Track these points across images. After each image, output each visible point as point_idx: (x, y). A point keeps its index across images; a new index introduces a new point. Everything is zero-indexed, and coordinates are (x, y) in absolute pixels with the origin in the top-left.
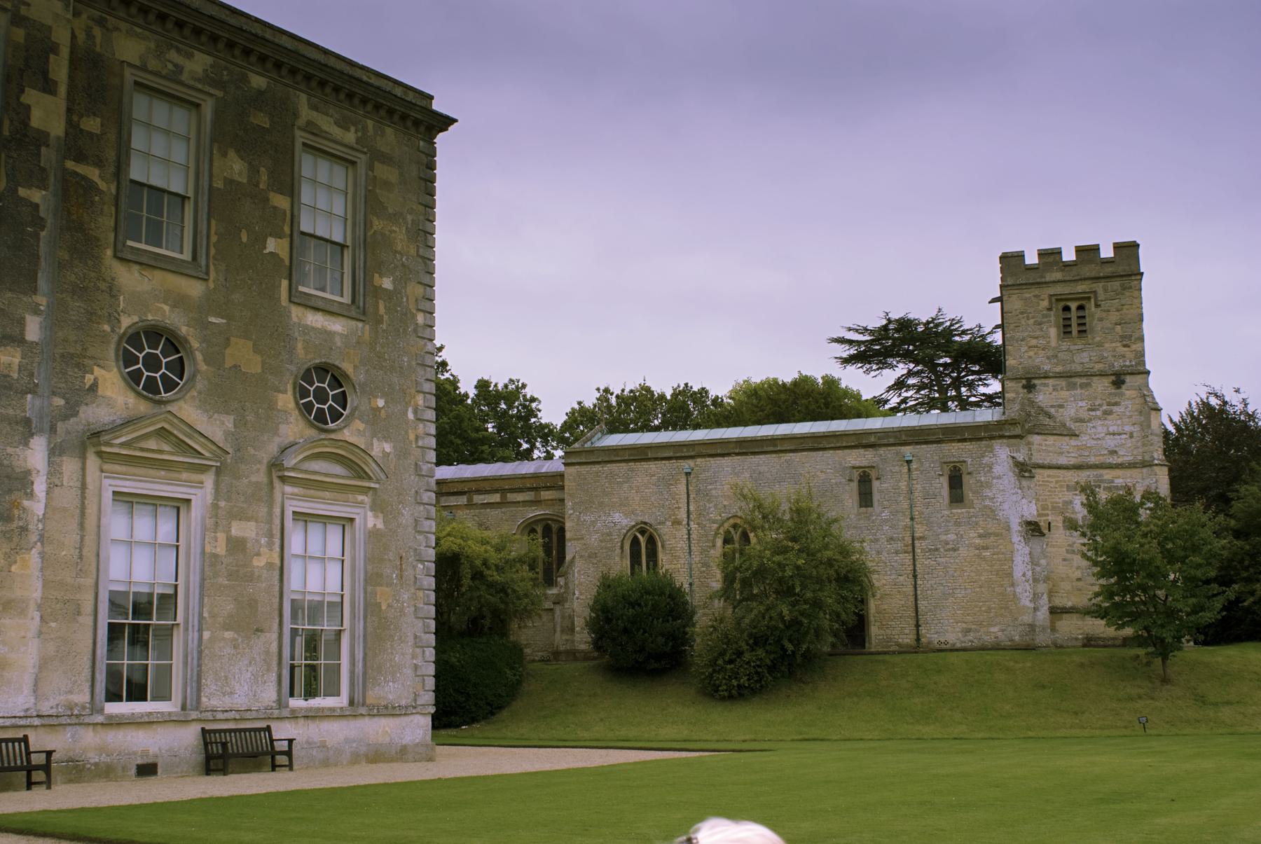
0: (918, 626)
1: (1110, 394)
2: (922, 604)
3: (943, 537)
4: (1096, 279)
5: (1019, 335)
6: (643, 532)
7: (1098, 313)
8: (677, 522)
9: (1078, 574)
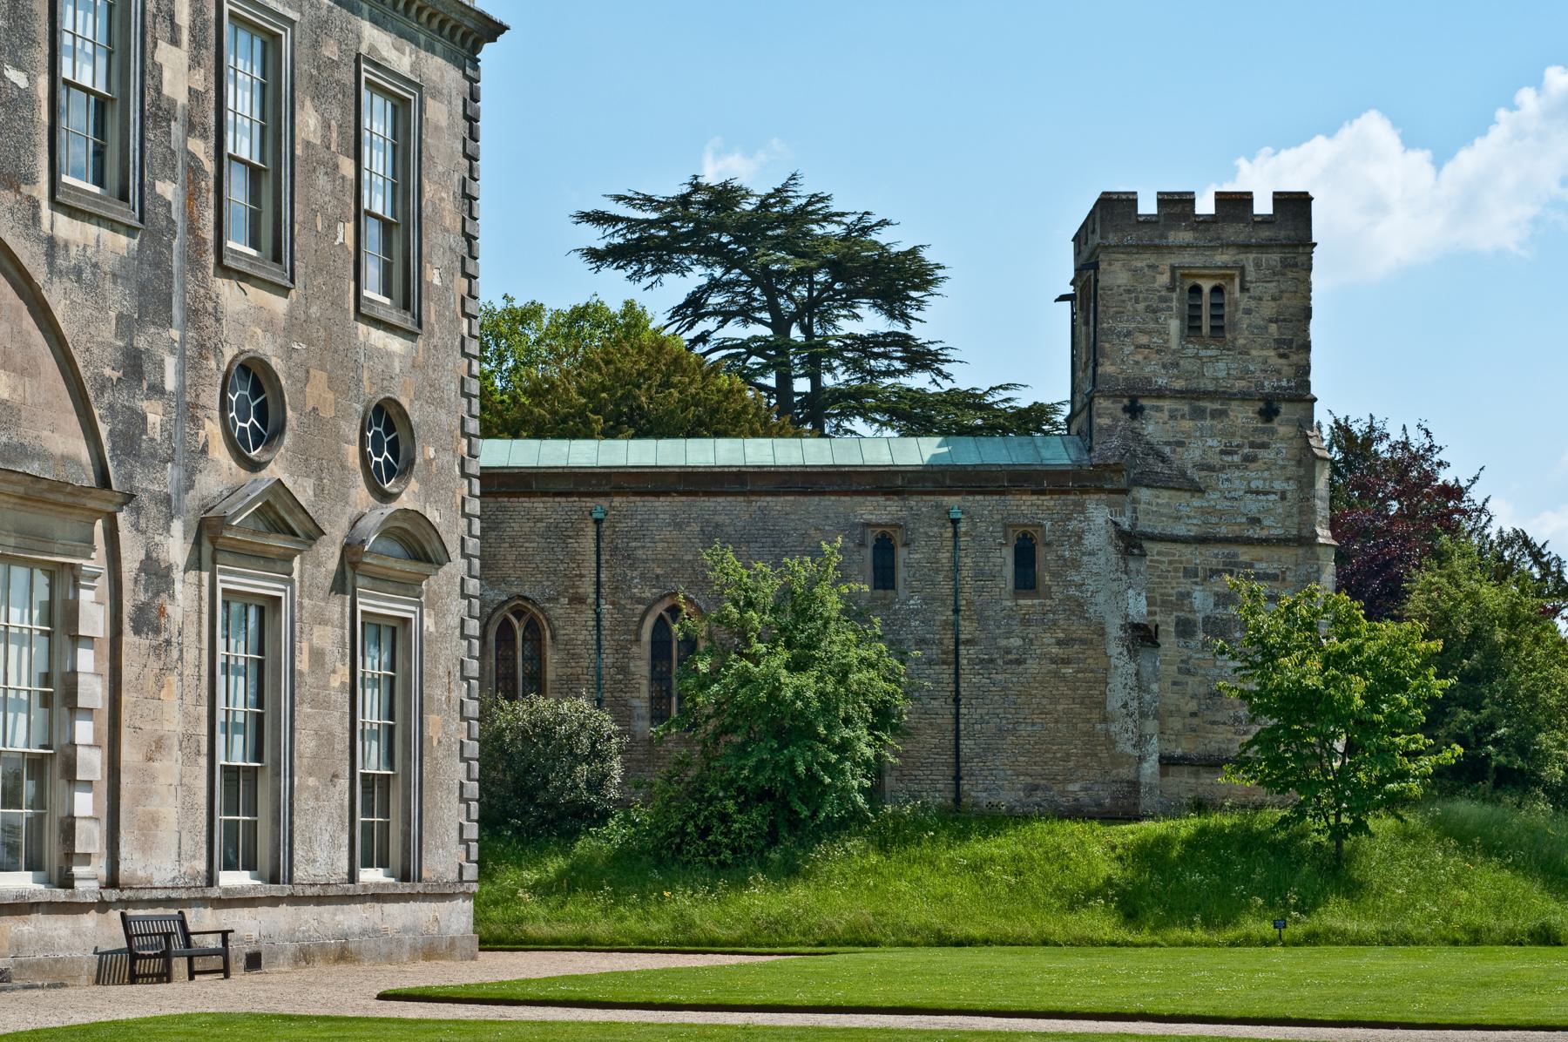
0: (957, 778)
1: (1255, 430)
2: (966, 745)
3: (1003, 643)
4: (1245, 247)
5: (1122, 326)
6: (518, 613)
7: (1245, 302)
8: (578, 600)
9: (1192, 706)
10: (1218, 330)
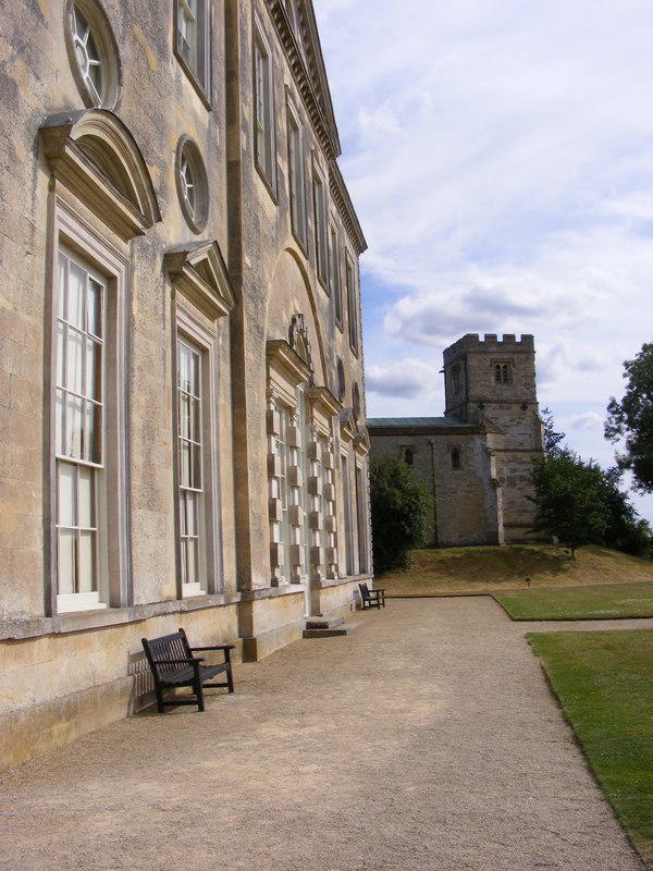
10: (506, 380)
